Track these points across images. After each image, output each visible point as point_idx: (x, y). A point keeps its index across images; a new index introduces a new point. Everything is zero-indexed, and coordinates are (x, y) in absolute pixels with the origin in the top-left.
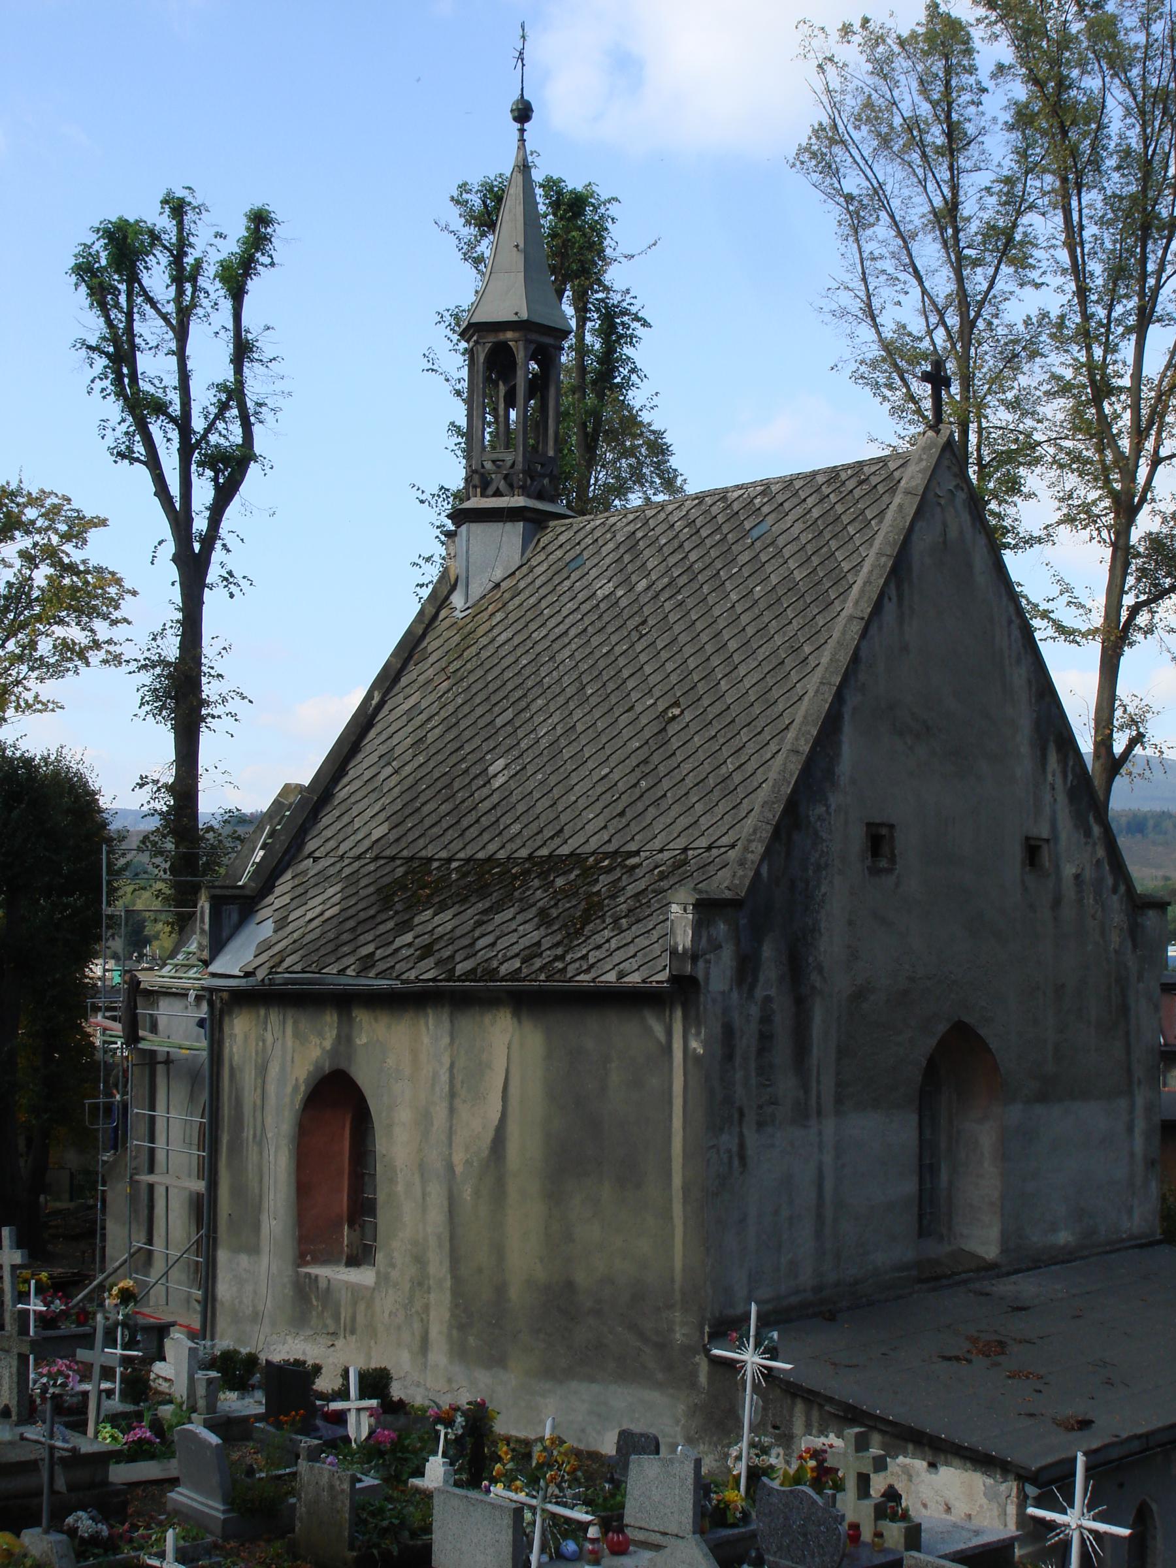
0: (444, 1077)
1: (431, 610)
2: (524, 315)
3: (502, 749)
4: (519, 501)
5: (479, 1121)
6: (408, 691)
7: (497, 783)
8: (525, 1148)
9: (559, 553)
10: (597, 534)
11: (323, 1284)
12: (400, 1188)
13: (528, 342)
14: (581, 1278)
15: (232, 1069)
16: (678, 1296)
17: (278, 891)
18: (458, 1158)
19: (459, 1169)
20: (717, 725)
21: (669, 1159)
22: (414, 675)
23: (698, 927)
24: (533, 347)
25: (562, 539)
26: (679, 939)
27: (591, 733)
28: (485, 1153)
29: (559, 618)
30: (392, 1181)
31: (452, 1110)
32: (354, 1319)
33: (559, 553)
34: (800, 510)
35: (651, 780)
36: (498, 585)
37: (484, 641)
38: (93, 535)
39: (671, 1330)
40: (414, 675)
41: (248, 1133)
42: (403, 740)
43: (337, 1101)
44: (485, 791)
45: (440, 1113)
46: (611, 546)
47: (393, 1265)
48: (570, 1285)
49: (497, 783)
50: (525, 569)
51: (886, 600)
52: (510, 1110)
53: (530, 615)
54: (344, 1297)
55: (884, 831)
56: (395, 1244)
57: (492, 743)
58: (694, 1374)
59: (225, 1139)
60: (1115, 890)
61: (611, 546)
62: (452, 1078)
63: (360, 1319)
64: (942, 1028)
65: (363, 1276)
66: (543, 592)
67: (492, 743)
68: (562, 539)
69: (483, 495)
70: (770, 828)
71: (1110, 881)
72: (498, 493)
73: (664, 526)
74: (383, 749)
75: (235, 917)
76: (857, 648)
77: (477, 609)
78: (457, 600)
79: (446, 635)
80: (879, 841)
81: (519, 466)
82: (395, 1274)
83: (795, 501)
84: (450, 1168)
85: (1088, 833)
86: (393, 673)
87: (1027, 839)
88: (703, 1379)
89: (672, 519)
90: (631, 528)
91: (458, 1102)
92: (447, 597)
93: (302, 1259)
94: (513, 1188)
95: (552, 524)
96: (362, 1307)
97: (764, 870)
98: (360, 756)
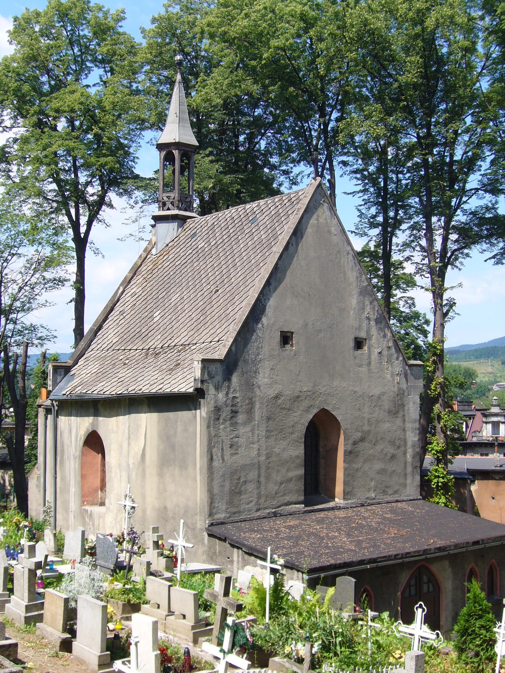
0: (127, 431)
1: (144, 255)
2: (177, 141)
3: (159, 307)
4: (176, 212)
5: (137, 447)
6: (133, 287)
7: (155, 320)
8: (152, 457)
9: (189, 232)
10: (202, 223)
11: (89, 511)
12: (113, 475)
13: (180, 150)
14: (169, 505)
15: (61, 432)
16: (198, 510)
17: (79, 364)
18: (131, 461)
19: (131, 466)
20: (228, 295)
21: (196, 458)
22: (135, 281)
23: (203, 369)
24: (182, 152)
25: (191, 226)
26: (197, 374)
27: (189, 300)
28: (139, 459)
29: (185, 257)
30: (111, 472)
31: (129, 444)
32: (99, 525)
33: (189, 232)
34: (268, 212)
35: (204, 316)
36: (168, 245)
37: (160, 267)
38: (468, 259)
39: (196, 523)
40: (135, 281)
41: (66, 456)
42: (129, 305)
43: (94, 442)
44: (152, 323)
45: (125, 444)
46: (206, 228)
47: (111, 504)
48: (165, 508)
49: (155, 320)
50: (177, 239)
51: (290, 245)
52: (147, 444)
53: (176, 256)
54: (95, 516)
55: (289, 334)
56: (112, 496)
57: (156, 305)
58: (203, 539)
59: (58, 459)
60: (397, 359)
61: (206, 228)
62: (129, 430)
63: (101, 525)
64: (315, 411)
65: (102, 509)
66: (182, 247)
67: (156, 305)
68: (191, 226)
69: (163, 210)
70: (236, 332)
71: (395, 356)
72: (169, 209)
73: (224, 220)
74: (121, 309)
75: (63, 373)
76: (277, 264)
77: (161, 254)
78: (154, 251)
79: (148, 264)
80: (286, 338)
81: (176, 199)
82: (112, 507)
83: (267, 208)
84: (128, 465)
85: (385, 336)
86: (128, 280)
87: (356, 338)
88: (206, 541)
89: (227, 217)
90: (213, 221)
91: (131, 440)
92: (151, 250)
93: (83, 503)
94: (147, 472)
95: (188, 220)
96: (101, 520)
97: (233, 348)
98: (113, 312)
